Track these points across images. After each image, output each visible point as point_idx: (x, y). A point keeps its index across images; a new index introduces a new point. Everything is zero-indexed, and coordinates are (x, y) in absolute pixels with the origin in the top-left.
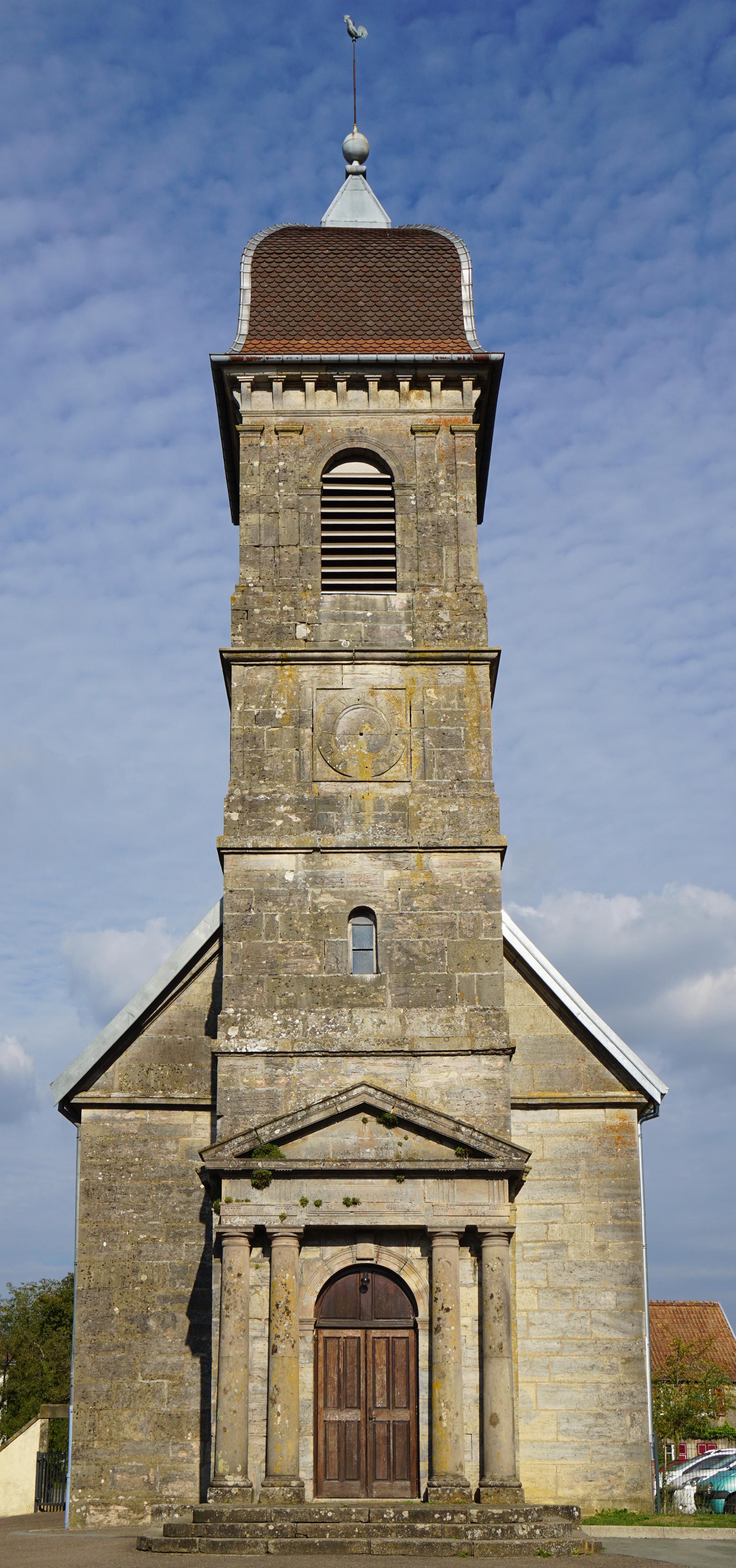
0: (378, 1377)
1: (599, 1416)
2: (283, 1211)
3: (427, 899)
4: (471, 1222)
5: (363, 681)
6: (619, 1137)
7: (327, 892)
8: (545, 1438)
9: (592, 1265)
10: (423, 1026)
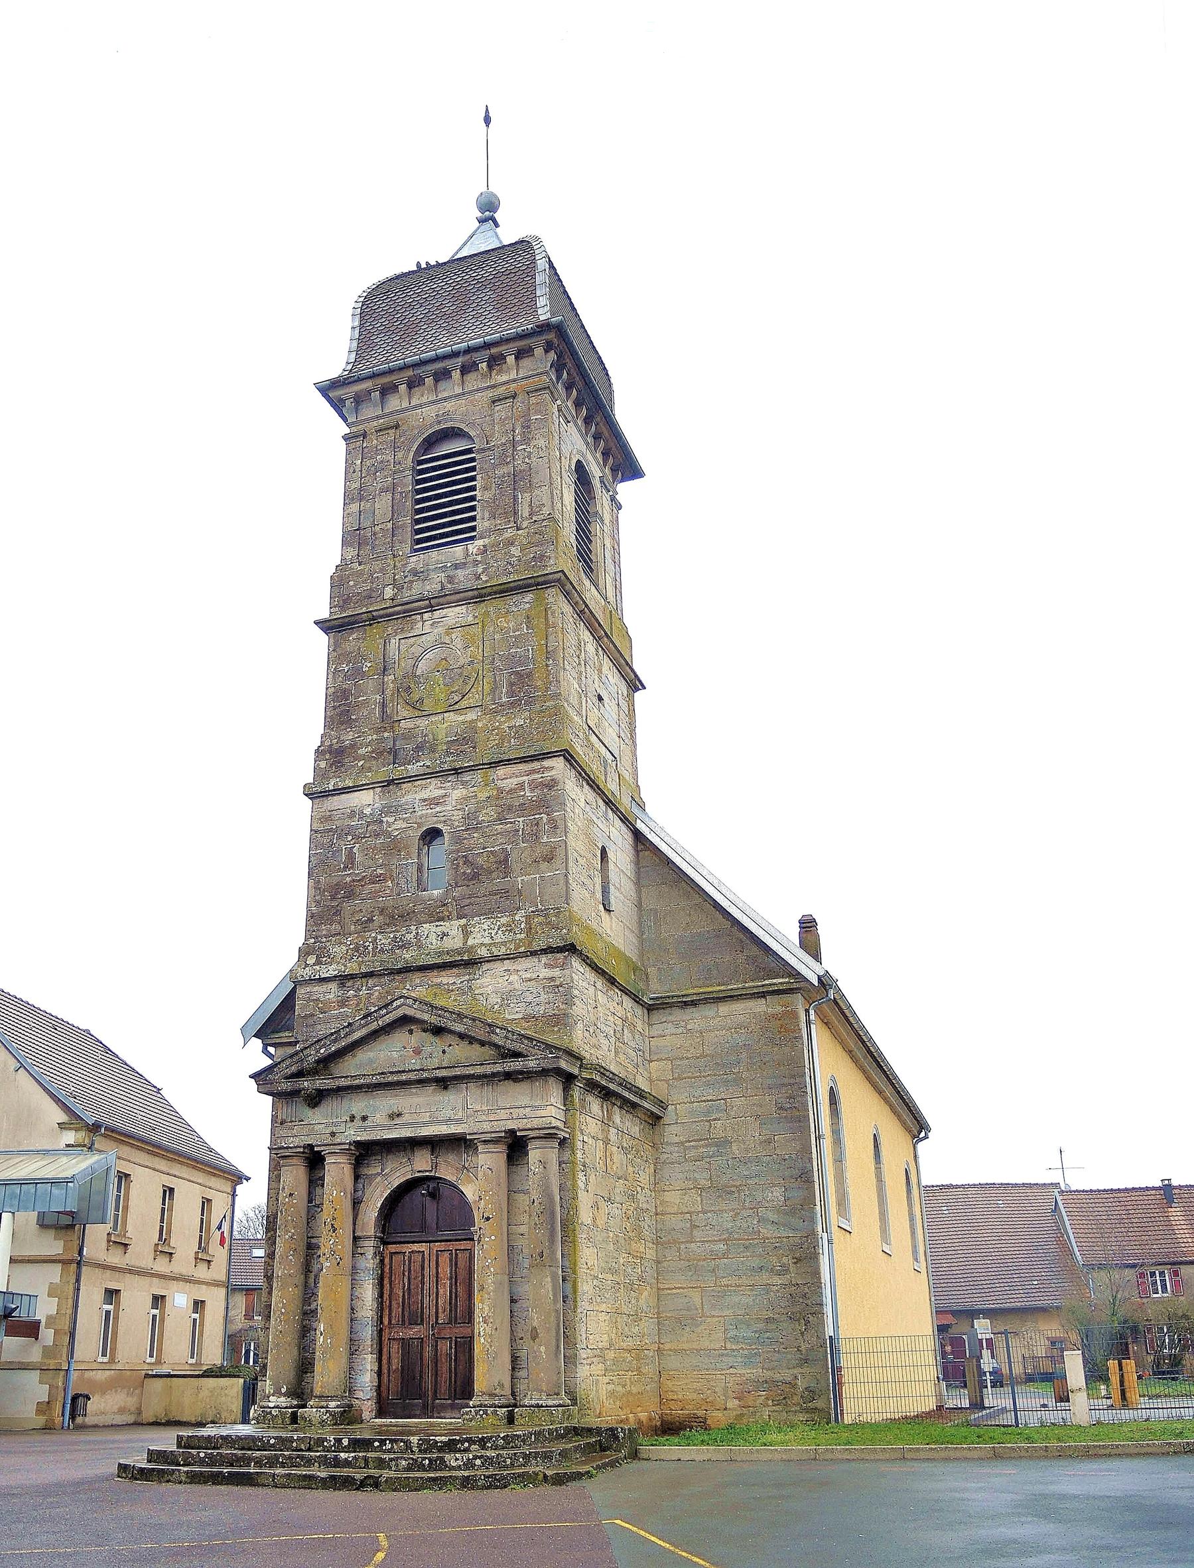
0: (441, 1291)
1: (768, 1320)
4: (511, 1125)
8: (712, 1346)
9: (758, 1160)
10: (484, 934)
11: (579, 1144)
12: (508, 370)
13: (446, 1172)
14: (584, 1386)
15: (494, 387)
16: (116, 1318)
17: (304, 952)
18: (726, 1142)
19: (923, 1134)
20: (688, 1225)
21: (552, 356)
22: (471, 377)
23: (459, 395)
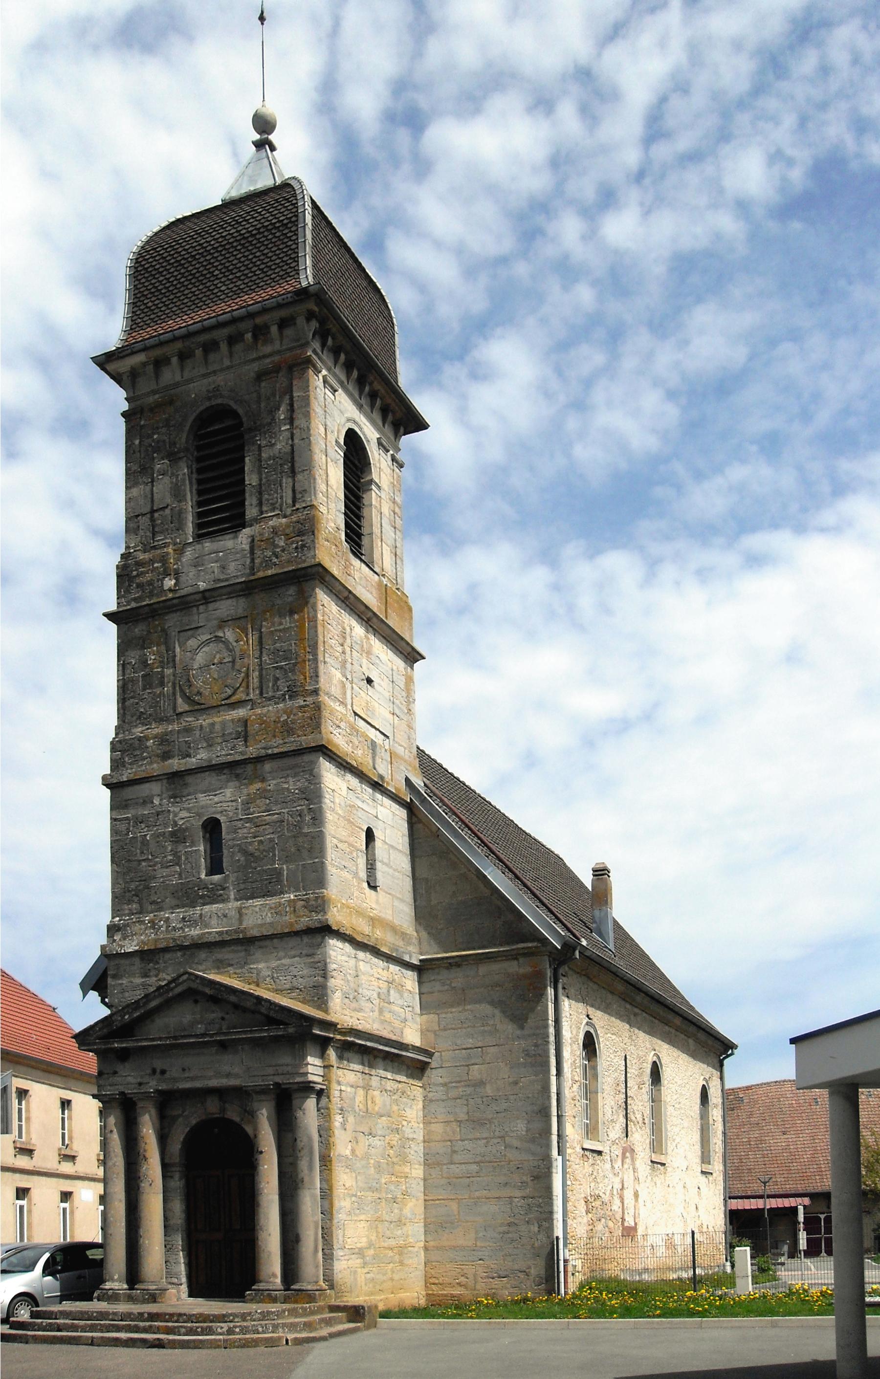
2: (139, 1080)
3: (262, 803)
5: (214, 617)
6: (531, 984)
7: (184, 809)
11: (337, 1094)
12: (272, 341)
13: (233, 1114)
14: (340, 1277)
15: (259, 358)
16: (30, 1211)
17: (112, 929)
18: (481, 1083)
19: (730, 1052)
20: (449, 1150)
21: (314, 324)
22: (239, 347)
23: (228, 368)
